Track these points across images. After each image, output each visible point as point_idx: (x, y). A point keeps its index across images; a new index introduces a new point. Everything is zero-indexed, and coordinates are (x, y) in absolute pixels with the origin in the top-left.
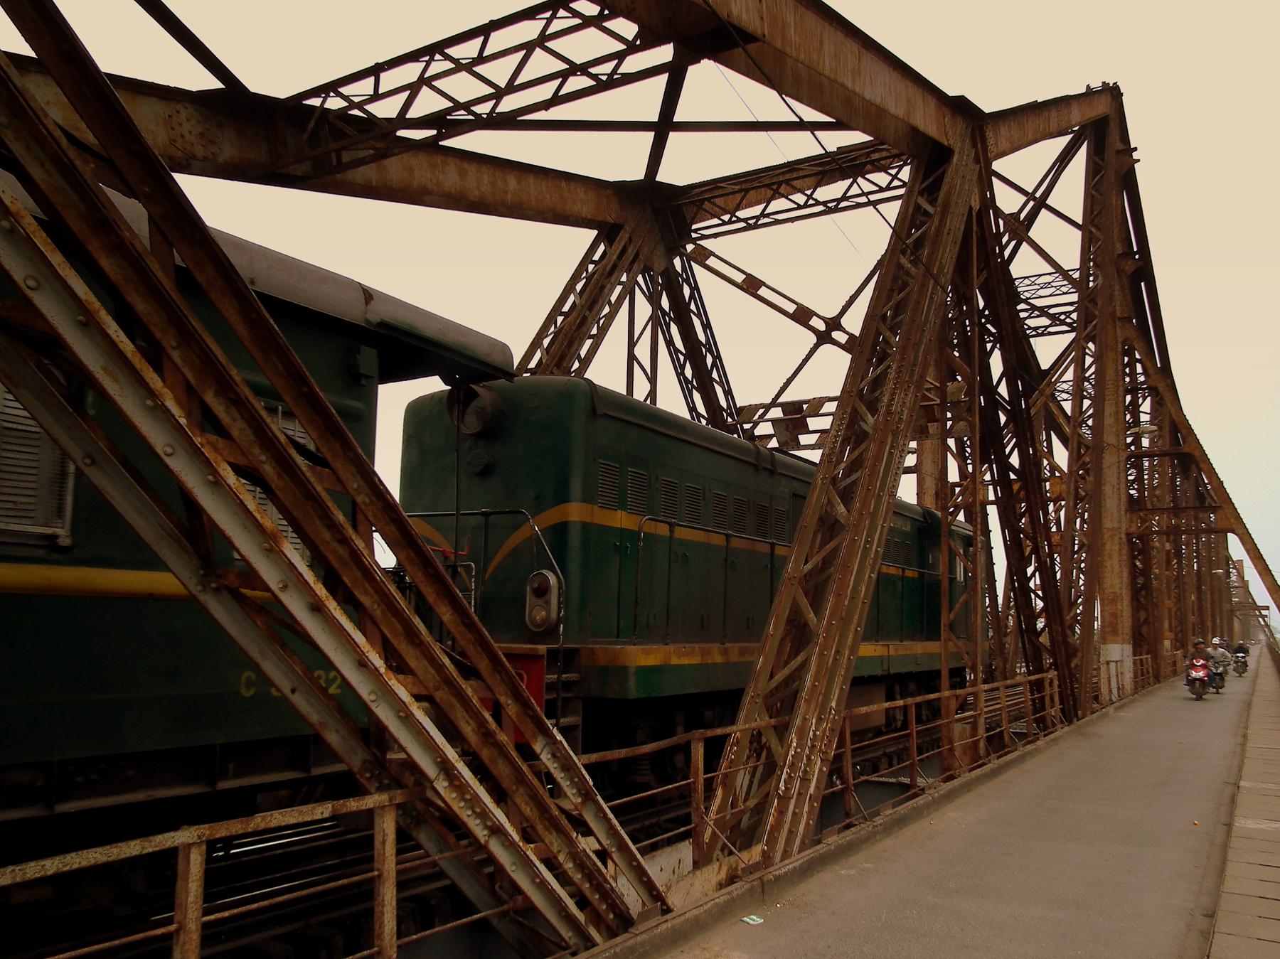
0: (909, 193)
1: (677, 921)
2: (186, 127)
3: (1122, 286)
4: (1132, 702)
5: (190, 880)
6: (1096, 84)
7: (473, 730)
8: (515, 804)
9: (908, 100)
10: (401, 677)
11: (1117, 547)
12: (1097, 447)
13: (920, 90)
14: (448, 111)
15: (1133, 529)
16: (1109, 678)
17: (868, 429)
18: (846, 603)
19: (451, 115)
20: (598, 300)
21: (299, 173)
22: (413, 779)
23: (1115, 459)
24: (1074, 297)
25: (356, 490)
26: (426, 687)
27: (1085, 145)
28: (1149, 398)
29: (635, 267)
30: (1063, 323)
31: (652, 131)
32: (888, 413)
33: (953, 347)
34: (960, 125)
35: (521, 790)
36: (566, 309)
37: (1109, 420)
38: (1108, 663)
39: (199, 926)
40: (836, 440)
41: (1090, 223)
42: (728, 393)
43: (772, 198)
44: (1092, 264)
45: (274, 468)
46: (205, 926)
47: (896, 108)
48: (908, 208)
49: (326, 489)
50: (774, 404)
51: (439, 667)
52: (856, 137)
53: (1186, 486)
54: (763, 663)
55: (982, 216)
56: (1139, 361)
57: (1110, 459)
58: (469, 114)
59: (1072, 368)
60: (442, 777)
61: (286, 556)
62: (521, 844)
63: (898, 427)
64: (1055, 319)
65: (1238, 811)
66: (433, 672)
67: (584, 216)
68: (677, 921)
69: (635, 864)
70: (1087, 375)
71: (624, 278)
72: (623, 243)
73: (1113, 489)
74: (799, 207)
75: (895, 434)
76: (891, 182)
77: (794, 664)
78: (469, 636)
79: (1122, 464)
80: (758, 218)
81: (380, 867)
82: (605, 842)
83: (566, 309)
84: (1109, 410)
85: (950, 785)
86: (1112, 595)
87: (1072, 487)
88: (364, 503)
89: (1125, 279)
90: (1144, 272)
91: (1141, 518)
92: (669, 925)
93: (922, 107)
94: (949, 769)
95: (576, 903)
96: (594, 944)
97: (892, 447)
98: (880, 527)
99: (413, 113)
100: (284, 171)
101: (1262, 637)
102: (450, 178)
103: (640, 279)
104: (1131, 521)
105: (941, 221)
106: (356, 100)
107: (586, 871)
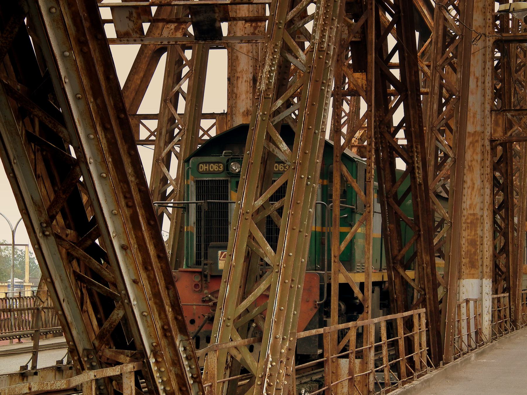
4: (491, 349)
11: (479, 157)
15: (499, 134)
16: (468, 320)
38: (467, 301)
40: (270, 75)
63: (326, 63)
79: (489, 50)
86: (471, 217)
104: (497, 123)
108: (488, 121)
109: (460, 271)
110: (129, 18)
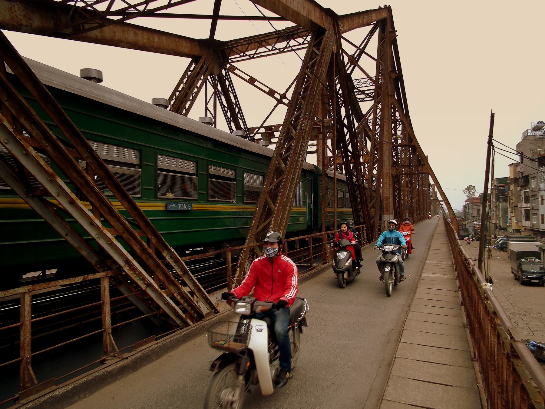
0: (310, 46)
1: (221, 316)
2: (18, 13)
3: (391, 83)
5: (26, 306)
6: (382, 6)
7: (138, 248)
8: (156, 275)
9: (308, 9)
10: (109, 229)
11: (388, 180)
12: (381, 143)
13: (313, 6)
14: (127, 9)
15: (394, 173)
17: (293, 136)
18: (285, 200)
19: (127, 10)
20: (192, 86)
21: (67, 33)
22: (116, 267)
23: (388, 148)
24: (373, 87)
25: (86, 157)
26: (119, 232)
27: (378, 30)
28: (401, 125)
29: (207, 73)
30: (370, 97)
31: (210, 19)
32: (301, 129)
33: (330, 106)
34: (329, 20)
35: (159, 270)
36: (180, 89)
37: (386, 133)
38: (384, 221)
39: (30, 323)
41: (380, 59)
42: (244, 122)
43: (259, 47)
44: (380, 75)
45: (51, 149)
46: (33, 323)
47: (303, 13)
48: (309, 51)
49: (74, 157)
50: (262, 127)
51: (124, 225)
52: (289, 24)
53: (414, 158)
54: (255, 223)
55: (338, 54)
56: (397, 111)
57: (386, 147)
58: (135, 10)
59: (372, 115)
60: (126, 266)
61: (58, 183)
62: (159, 290)
64: (368, 95)
65: (424, 271)
66: (121, 227)
67: (186, 52)
68: (221, 316)
69: (204, 296)
70: (378, 116)
71: (202, 77)
72: (201, 64)
74: (270, 51)
75: (303, 137)
76: (304, 41)
77: (266, 223)
78: (135, 213)
80: (254, 55)
81: (103, 299)
82: (193, 288)
83: (180, 89)
84: (386, 129)
85: (325, 265)
87: (372, 158)
88: (91, 163)
89: (392, 81)
90: (399, 78)
91: (397, 169)
92: (217, 317)
93: (314, 11)
94: (324, 260)
95: (183, 312)
96: (189, 325)
97: (302, 142)
98: (297, 172)
99: (113, 9)
100: (61, 32)
101: (441, 212)
102: (131, 36)
103: (209, 78)
104: (393, 170)
105: (321, 57)
106: (89, 3)
107: (185, 299)
108: (391, 169)
109: (383, 212)
110: (266, 136)
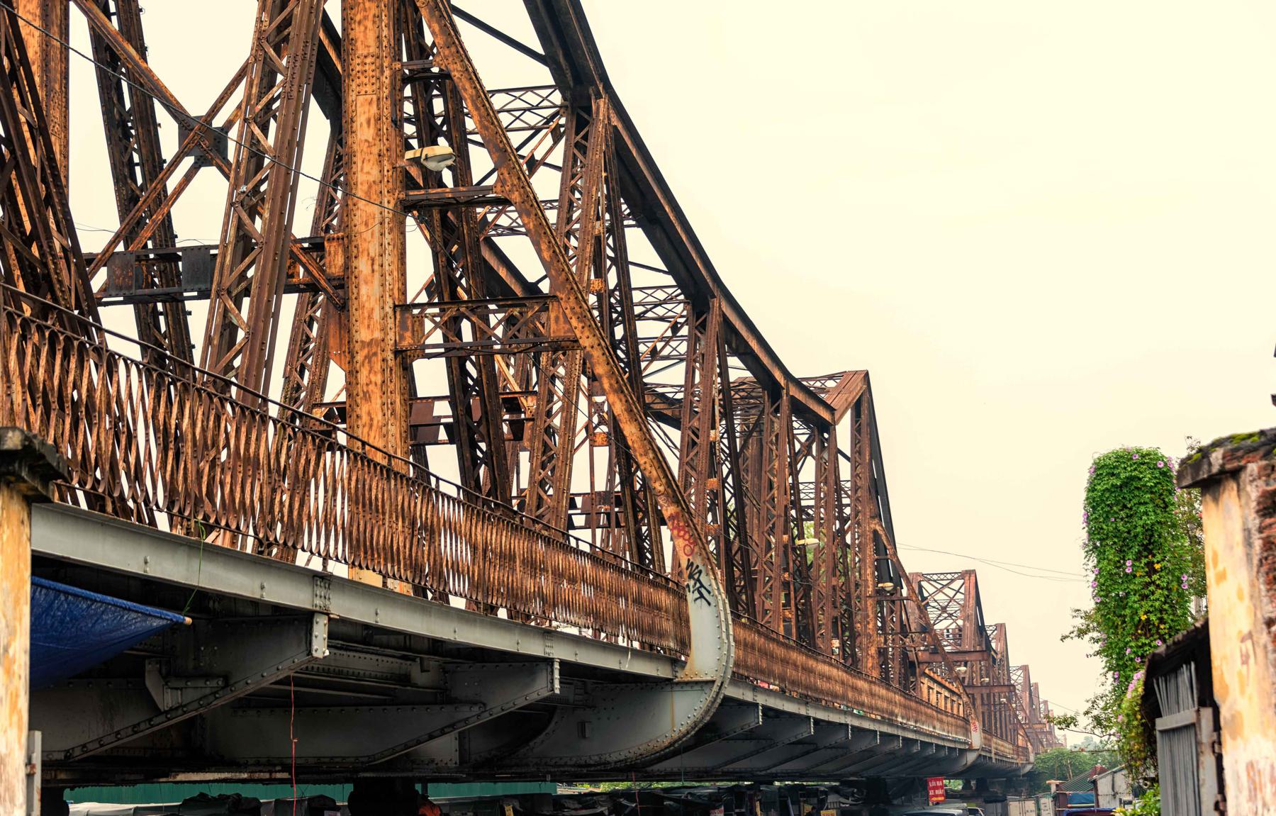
73: (373, 264)
